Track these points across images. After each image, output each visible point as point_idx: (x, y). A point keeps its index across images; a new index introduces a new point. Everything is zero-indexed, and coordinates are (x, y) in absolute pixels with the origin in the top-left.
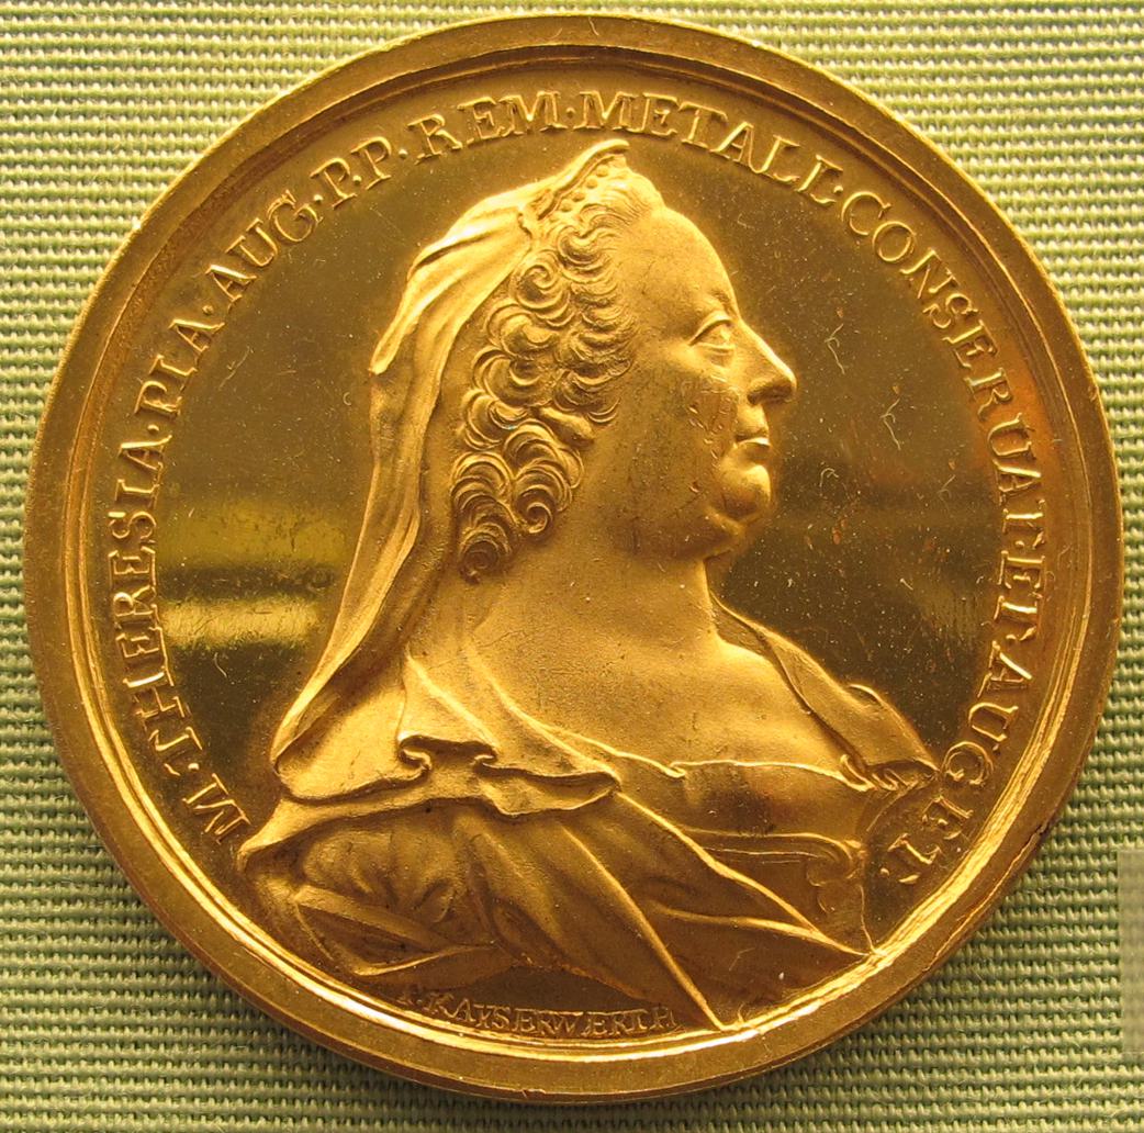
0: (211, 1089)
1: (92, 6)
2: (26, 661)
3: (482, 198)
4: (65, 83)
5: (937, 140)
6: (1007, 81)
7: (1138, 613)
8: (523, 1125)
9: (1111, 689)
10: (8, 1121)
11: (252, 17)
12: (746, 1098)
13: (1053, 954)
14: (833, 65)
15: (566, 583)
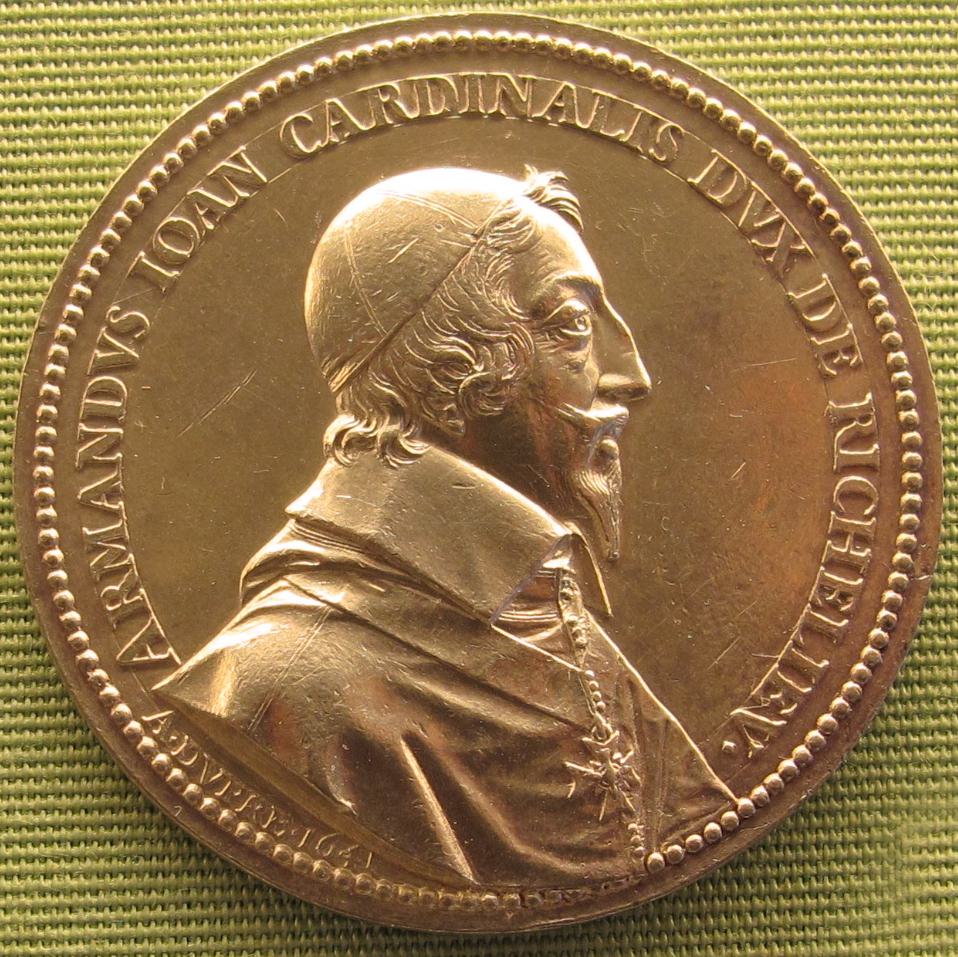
0: (114, 849)
3: (326, 429)
6: (854, 115)
7: (952, 202)
10: (6, 950)
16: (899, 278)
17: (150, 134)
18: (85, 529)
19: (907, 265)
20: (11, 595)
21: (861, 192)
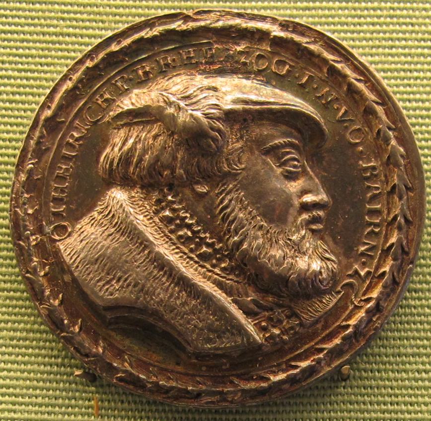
1: (292, 4)
2: (11, 254)
4: (389, 40)
5: (353, 47)
8: (284, 412)
9: (411, 278)
11: (406, 9)
12: (304, 409)
13: (398, 385)
14: (326, 27)
15: (16, 194)
16: (411, 127)
17: (80, 51)
18: (366, 217)
19: (411, 112)
20: (5, 253)
21: (395, 89)
